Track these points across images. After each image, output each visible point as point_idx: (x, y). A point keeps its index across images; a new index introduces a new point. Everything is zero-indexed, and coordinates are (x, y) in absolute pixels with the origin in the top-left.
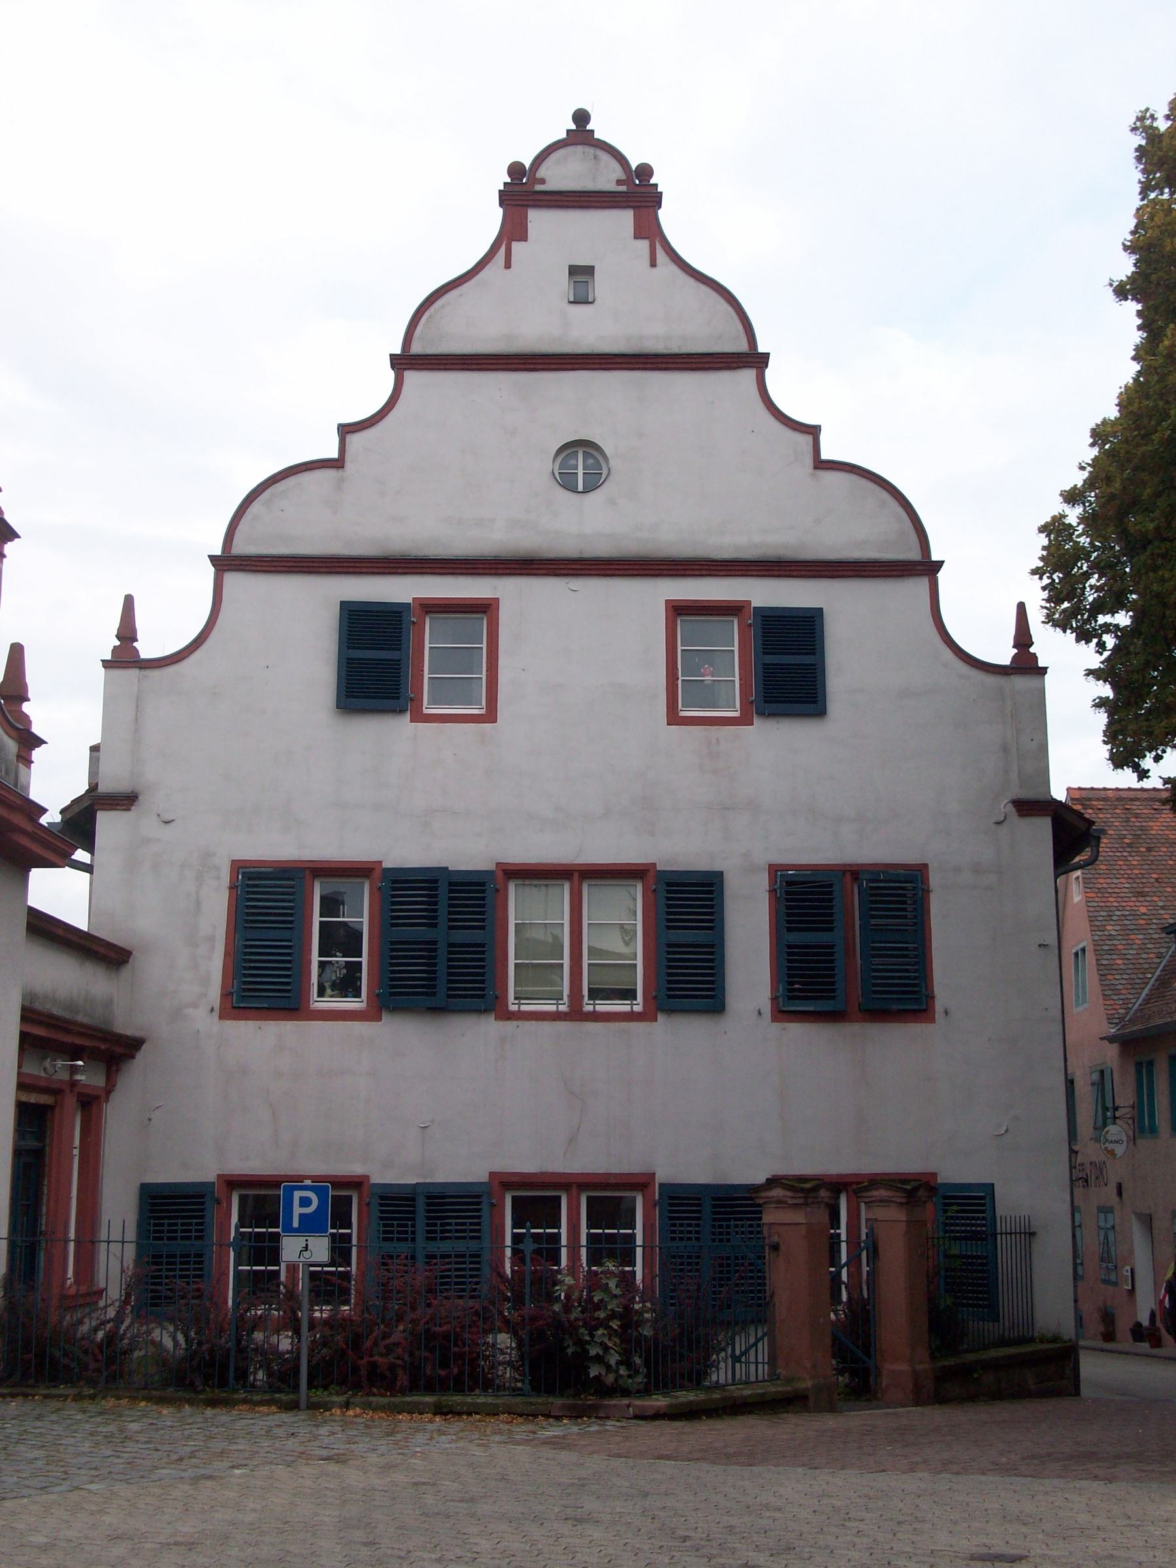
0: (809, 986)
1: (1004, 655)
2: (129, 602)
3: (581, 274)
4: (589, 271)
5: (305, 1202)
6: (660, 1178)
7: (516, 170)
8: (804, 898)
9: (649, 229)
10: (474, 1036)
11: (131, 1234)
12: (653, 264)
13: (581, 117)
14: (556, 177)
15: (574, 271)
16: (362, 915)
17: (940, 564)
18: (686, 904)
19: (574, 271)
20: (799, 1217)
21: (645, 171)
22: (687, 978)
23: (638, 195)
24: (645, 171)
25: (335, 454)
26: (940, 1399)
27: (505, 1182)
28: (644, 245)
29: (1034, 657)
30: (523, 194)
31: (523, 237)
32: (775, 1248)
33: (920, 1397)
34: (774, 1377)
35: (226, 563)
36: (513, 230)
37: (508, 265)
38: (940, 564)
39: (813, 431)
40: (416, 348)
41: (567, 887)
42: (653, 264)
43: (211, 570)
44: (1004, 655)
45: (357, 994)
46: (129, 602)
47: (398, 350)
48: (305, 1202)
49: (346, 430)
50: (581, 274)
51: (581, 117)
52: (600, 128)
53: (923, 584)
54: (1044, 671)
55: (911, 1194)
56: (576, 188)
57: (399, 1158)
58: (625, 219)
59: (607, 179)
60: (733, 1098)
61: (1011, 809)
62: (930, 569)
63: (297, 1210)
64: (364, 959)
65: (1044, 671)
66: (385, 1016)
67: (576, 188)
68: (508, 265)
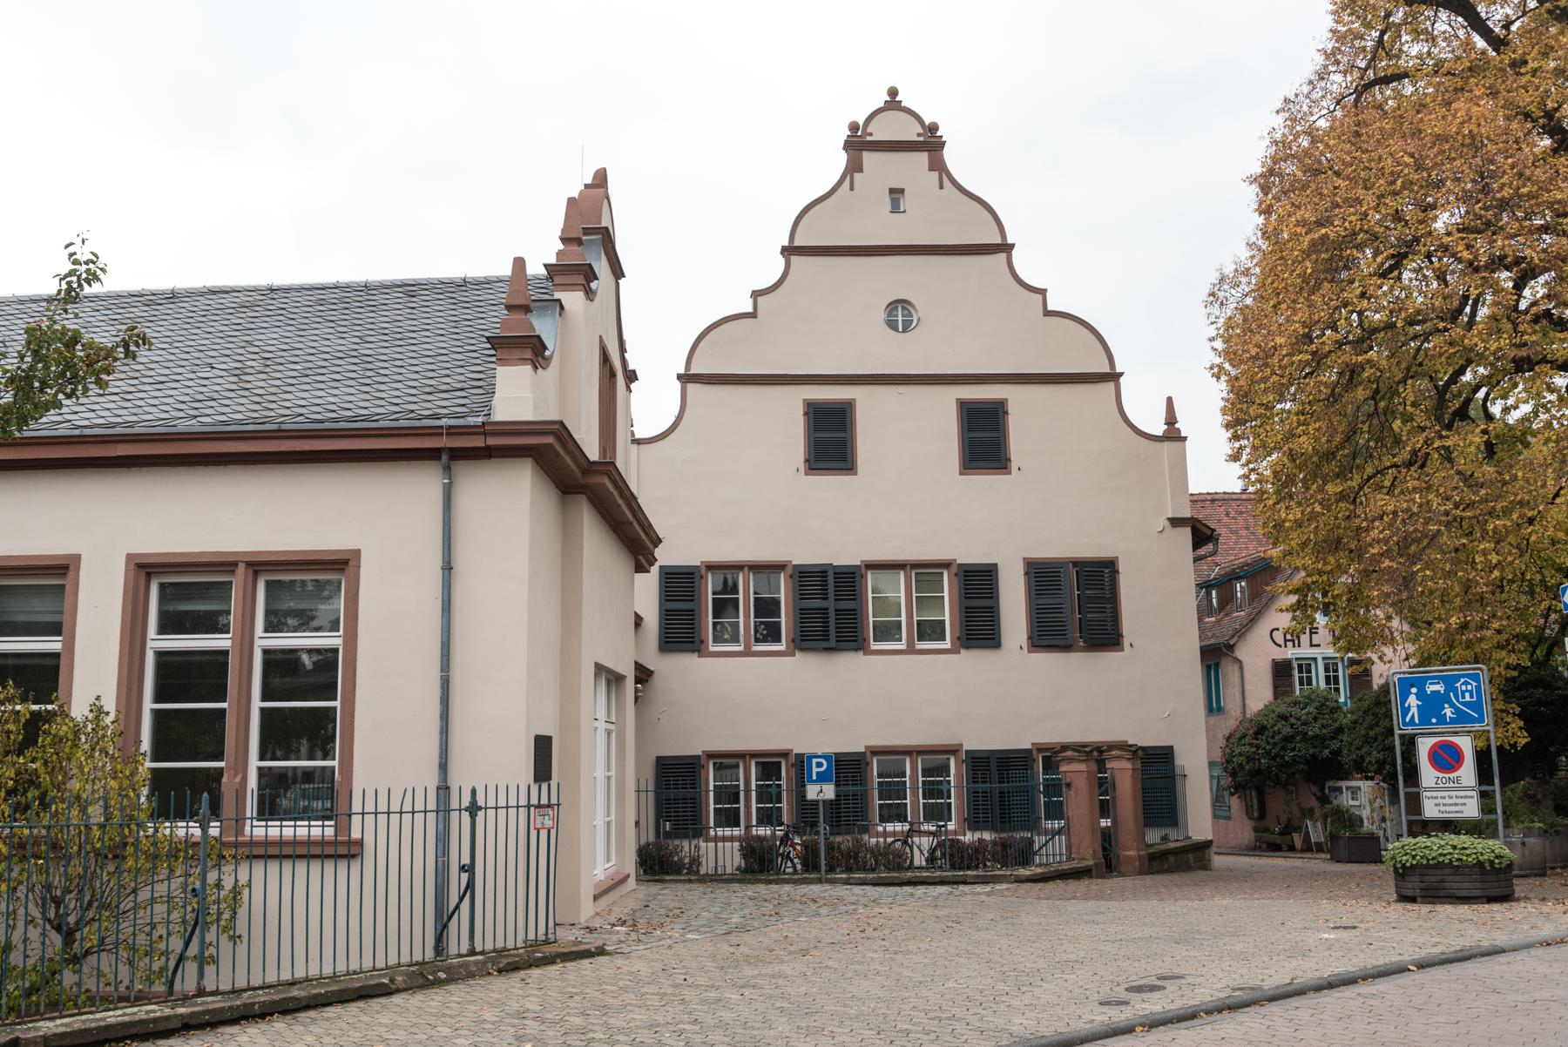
0: (1047, 634)
1: (1159, 429)
2: (1170, 400)
3: (896, 193)
4: (902, 191)
5: (819, 765)
6: (965, 748)
7: (854, 127)
8: (1042, 575)
9: (938, 166)
10: (848, 664)
11: (651, 787)
12: (941, 187)
13: (893, 92)
14: (879, 133)
15: (892, 191)
16: (783, 592)
17: (1121, 374)
18: (978, 584)
19: (892, 191)
20: (1082, 767)
21: (933, 128)
22: (979, 629)
23: (930, 144)
24: (933, 128)
25: (750, 310)
26: (1150, 871)
27: (1041, 748)
28: (936, 174)
29: (1179, 431)
30: (858, 144)
31: (860, 170)
32: (1068, 785)
33: (1142, 872)
34: (1070, 858)
35: (686, 379)
36: (854, 167)
37: (852, 188)
38: (1121, 374)
39: (1043, 292)
40: (797, 243)
41: (902, 574)
42: (941, 187)
43: (678, 385)
44: (1159, 429)
45: (779, 640)
46: (1170, 400)
47: (786, 244)
48: (819, 765)
49: (756, 295)
50: (896, 193)
51: (893, 92)
52: (905, 98)
53: (1112, 385)
54: (1185, 439)
55: (1135, 752)
56: (894, 142)
57: (821, 738)
58: (923, 157)
59: (911, 133)
60: (1015, 697)
61: (1167, 523)
62: (1114, 377)
63: (815, 770)
64: (783, 620)
65: (1185, 439)
66: (798, 654)
67: (894, 142)
68: (852, 188)
